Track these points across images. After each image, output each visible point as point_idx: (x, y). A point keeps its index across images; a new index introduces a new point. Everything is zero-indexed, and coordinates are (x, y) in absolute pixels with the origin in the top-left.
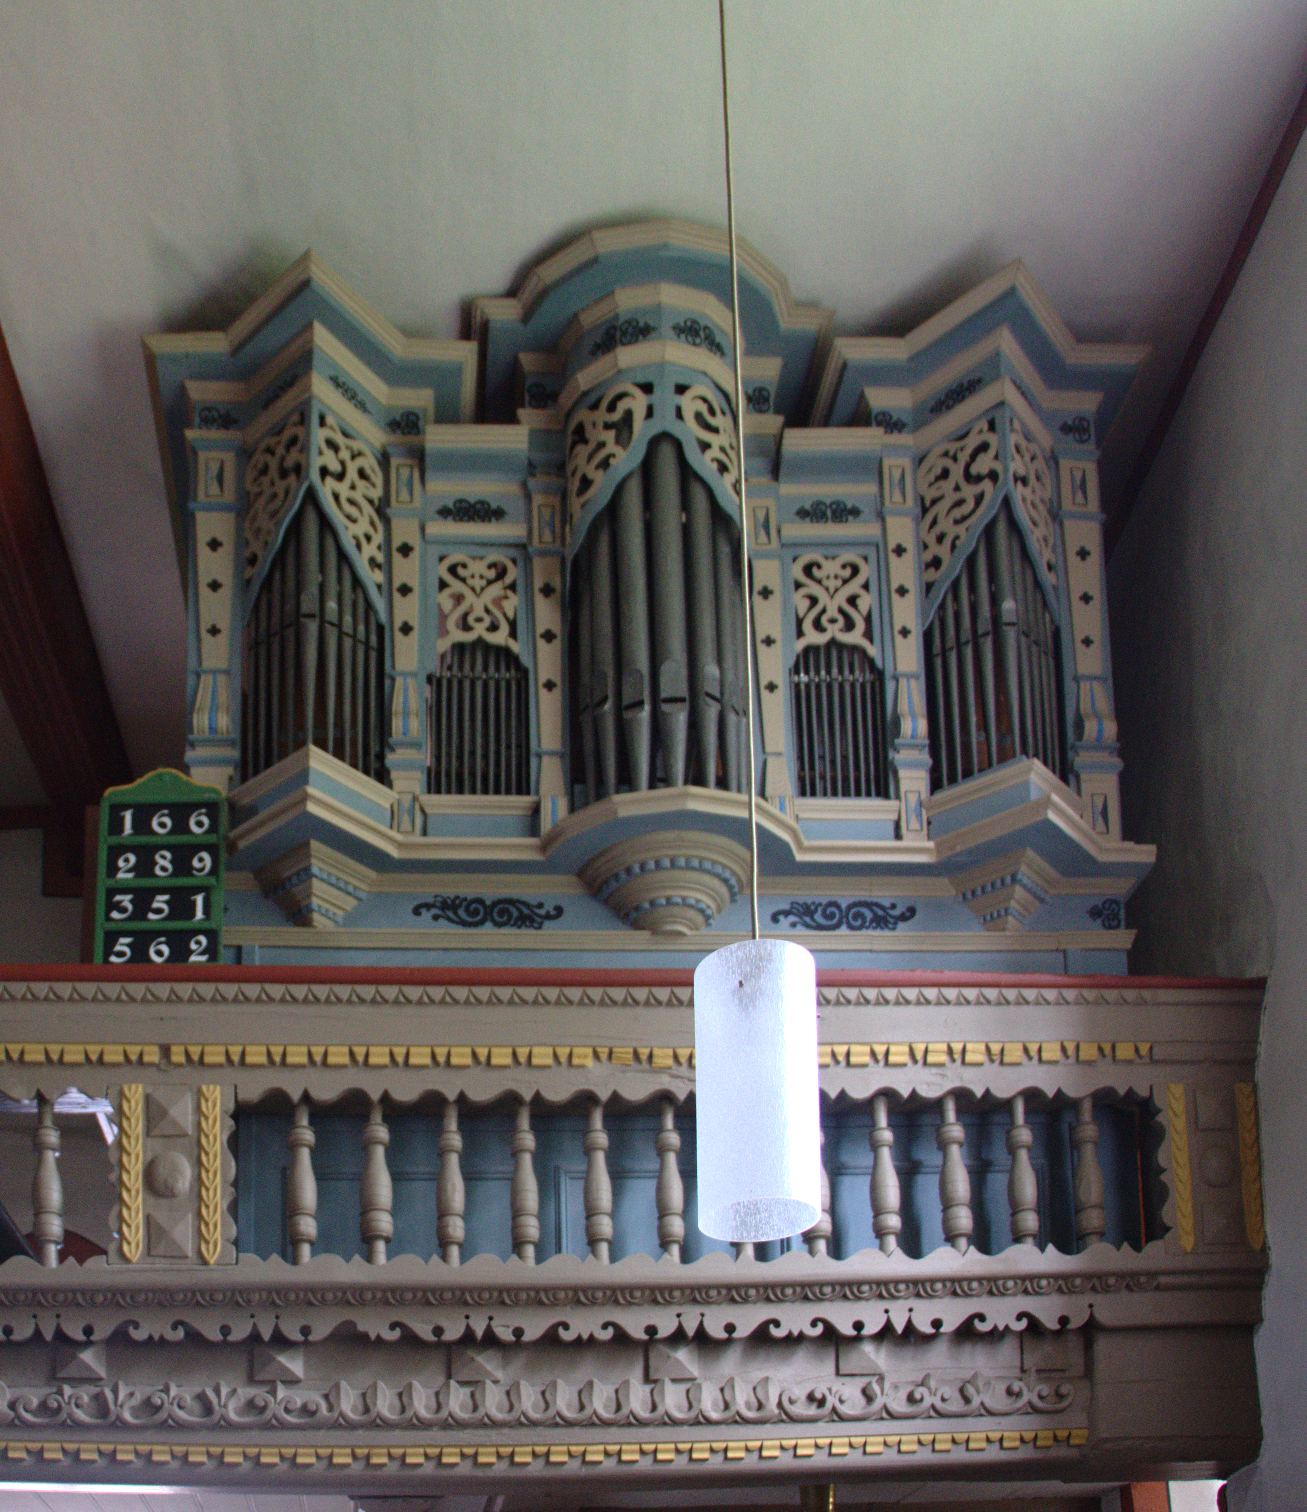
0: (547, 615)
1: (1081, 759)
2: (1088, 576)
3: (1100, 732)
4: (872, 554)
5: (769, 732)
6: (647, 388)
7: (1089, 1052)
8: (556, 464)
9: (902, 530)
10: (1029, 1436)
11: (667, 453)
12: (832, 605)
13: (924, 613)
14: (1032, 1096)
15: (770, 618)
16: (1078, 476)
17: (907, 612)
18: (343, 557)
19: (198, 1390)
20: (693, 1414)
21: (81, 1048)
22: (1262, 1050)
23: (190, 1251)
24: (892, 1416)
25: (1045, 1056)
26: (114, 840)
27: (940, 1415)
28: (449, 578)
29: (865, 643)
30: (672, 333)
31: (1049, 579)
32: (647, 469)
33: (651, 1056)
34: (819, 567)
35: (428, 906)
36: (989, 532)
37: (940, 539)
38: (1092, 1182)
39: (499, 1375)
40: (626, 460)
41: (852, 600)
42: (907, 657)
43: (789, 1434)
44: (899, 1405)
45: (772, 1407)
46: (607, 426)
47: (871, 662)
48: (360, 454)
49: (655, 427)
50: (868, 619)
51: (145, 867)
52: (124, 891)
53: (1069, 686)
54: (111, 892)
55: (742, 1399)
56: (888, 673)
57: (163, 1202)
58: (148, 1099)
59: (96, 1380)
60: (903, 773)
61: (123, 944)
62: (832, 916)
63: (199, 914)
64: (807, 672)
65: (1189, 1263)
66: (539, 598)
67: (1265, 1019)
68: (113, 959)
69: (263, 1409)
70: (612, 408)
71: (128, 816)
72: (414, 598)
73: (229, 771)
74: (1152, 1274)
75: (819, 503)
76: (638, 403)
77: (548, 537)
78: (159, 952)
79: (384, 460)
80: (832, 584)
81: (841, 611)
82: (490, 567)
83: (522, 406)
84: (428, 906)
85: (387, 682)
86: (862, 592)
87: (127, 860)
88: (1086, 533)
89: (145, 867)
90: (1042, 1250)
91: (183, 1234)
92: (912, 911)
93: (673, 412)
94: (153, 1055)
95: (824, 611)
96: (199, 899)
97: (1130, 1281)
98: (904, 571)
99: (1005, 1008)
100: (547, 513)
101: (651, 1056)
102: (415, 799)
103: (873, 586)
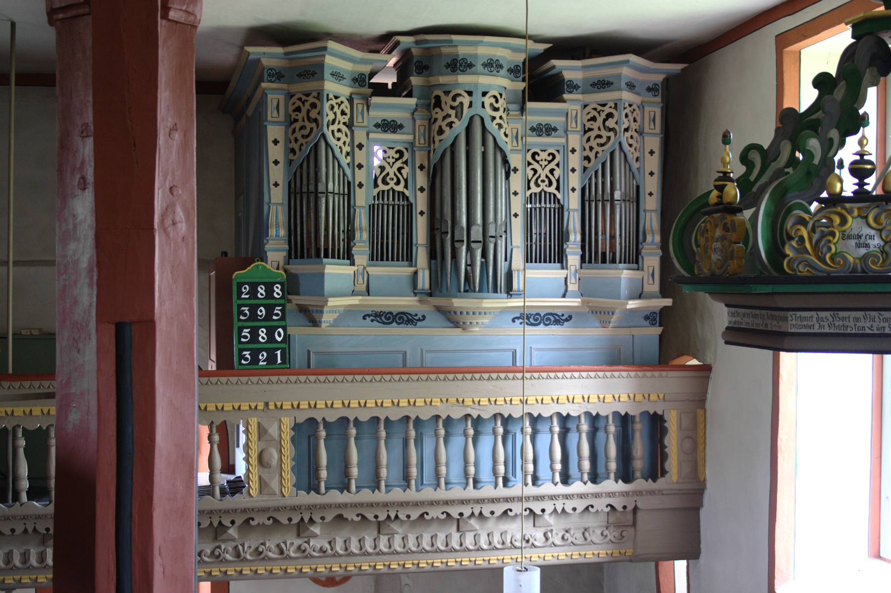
0: (421, 179)
2: (653, 163)
3: (653, 240)
6: (470, 93)
7: (639, 397)
8: (433, 129)
9: (575, 140)
11: (477, 122)
12: (543, 173)
13: (582, 181)
14: (616, 414)
17: (575, 181)
19: (277, 542)
20: (476, 547)
21: (231, 404)
22: (709, 396)
23: (277, 492)
31: (635, 166)
33: (463, 401)
35: (369, 315)
38: (639, 448)
39: (399, 531)
40: (460, 127)
41: (552, 171)
42: (574, 202)
44: (558, 541)
45: (508, 544)
46: (452, 108)
49: (473, 112)
50: (558, 181)
53: (642, 213)
56: (565, 209)
57: (266, 470)
58: (259, 424)
59: (233, 540)
60: (569, 257)
62: (537, 319)
64: (531, 203)
65: (675, 487)
66: (418, 170)
67: (711, 383)
69: (304, 551)
70: (454, 99)
73: (285, 254)
74: (660, 491)
76: (466, 100)
77: (422, 141)
79: (350, 100)
80: (544, 163)
82: (396, 152)
83: (413, 75)
84: (369, 315)
85: (352, 210)
86: (556, 168)
87: (263, 355)
88: (654, 143)
90: (617, 482)
91: (274, 484)
94: (261, 406)
95: (539, 177)
97: (652, 493)
98: (575, 161)
99: (606, 380)
100: (422, 129)
101: (463, 401)
102: (364, 268)
103: (561, 165)
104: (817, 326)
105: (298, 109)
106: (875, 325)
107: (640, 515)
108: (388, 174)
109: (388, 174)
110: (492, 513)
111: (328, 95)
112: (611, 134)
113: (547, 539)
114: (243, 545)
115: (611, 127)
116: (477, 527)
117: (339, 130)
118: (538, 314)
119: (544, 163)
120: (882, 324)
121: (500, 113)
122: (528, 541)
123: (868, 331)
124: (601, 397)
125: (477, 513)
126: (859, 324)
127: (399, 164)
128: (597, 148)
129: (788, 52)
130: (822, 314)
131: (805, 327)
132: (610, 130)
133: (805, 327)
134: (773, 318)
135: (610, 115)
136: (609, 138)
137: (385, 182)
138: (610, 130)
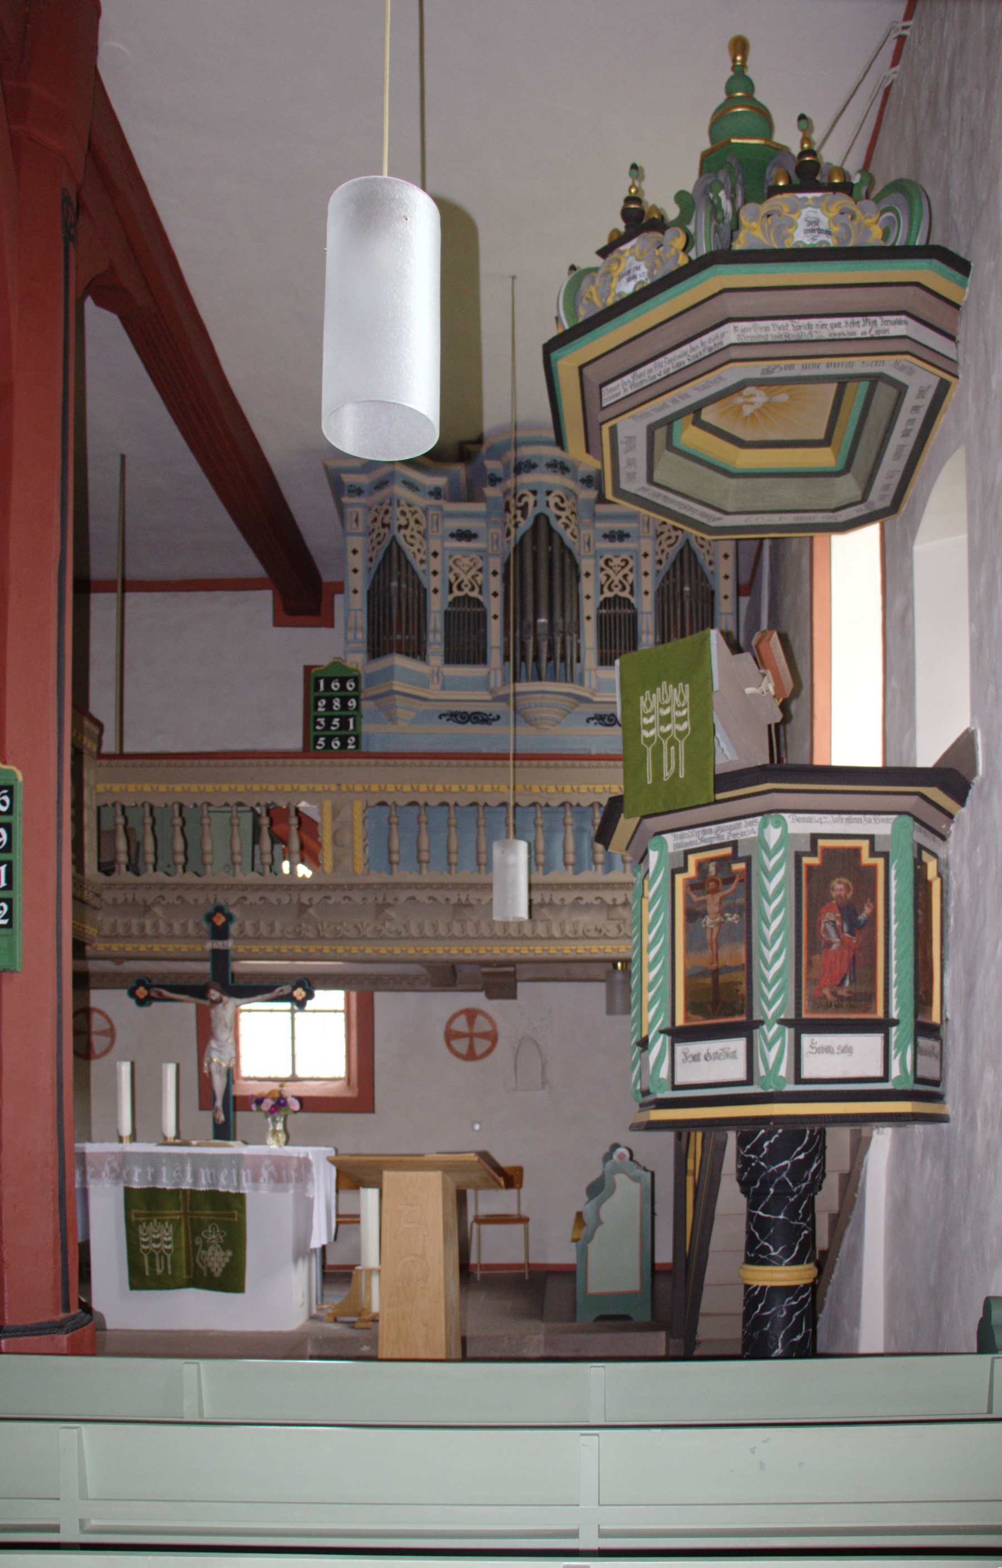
6: (534, 493)
12: (616, 578)
15: (587, 586)
17: (649, 584)
18: (407, 562)
26: (317, 694)
28: (453, 566)
30: (545, 468)
34: (611, 561)
36: (681, 552)
37: (663, 551)
41: (625, 576)
45: (580, 933)
46: (517, 508)
48: (416, 512)
49: (538, 510)
50: (632, 586)
51: (329, 706)
52: (321, 717)
54: (316, 718)
61: (321, 741)
63: (351, 727)
68: (318, 747)
69: (380, 931)
70: (520, 500)
71: (322, 682)
72: (438, 577)
75: (612, 532)
76: (530, 499)
78: (336, 744)
80: (617, 569)
81: (620, 582)
83: (485, 486)
89: (329, 706)
93: (545, 504)
94: (334, 788)
96: (351, 720)
98: (647, 565)
101: (530, 788)
102: (439, 668)
103: (635, 570)
105: (375, 520)
106: (662, 369)
108: (462, 581)
109: (462, 581)
111: (398, 502)
112: (679, 533)
113: (620, 930)
114: (322, 924)
117: (412, 537)
119: (617, 569)
121: (567, 513)
123: (658, 378)
127: (473, 572)
131: (614, 396)
133: (614, 396)
136: (677, 537)
137: (459, 588)
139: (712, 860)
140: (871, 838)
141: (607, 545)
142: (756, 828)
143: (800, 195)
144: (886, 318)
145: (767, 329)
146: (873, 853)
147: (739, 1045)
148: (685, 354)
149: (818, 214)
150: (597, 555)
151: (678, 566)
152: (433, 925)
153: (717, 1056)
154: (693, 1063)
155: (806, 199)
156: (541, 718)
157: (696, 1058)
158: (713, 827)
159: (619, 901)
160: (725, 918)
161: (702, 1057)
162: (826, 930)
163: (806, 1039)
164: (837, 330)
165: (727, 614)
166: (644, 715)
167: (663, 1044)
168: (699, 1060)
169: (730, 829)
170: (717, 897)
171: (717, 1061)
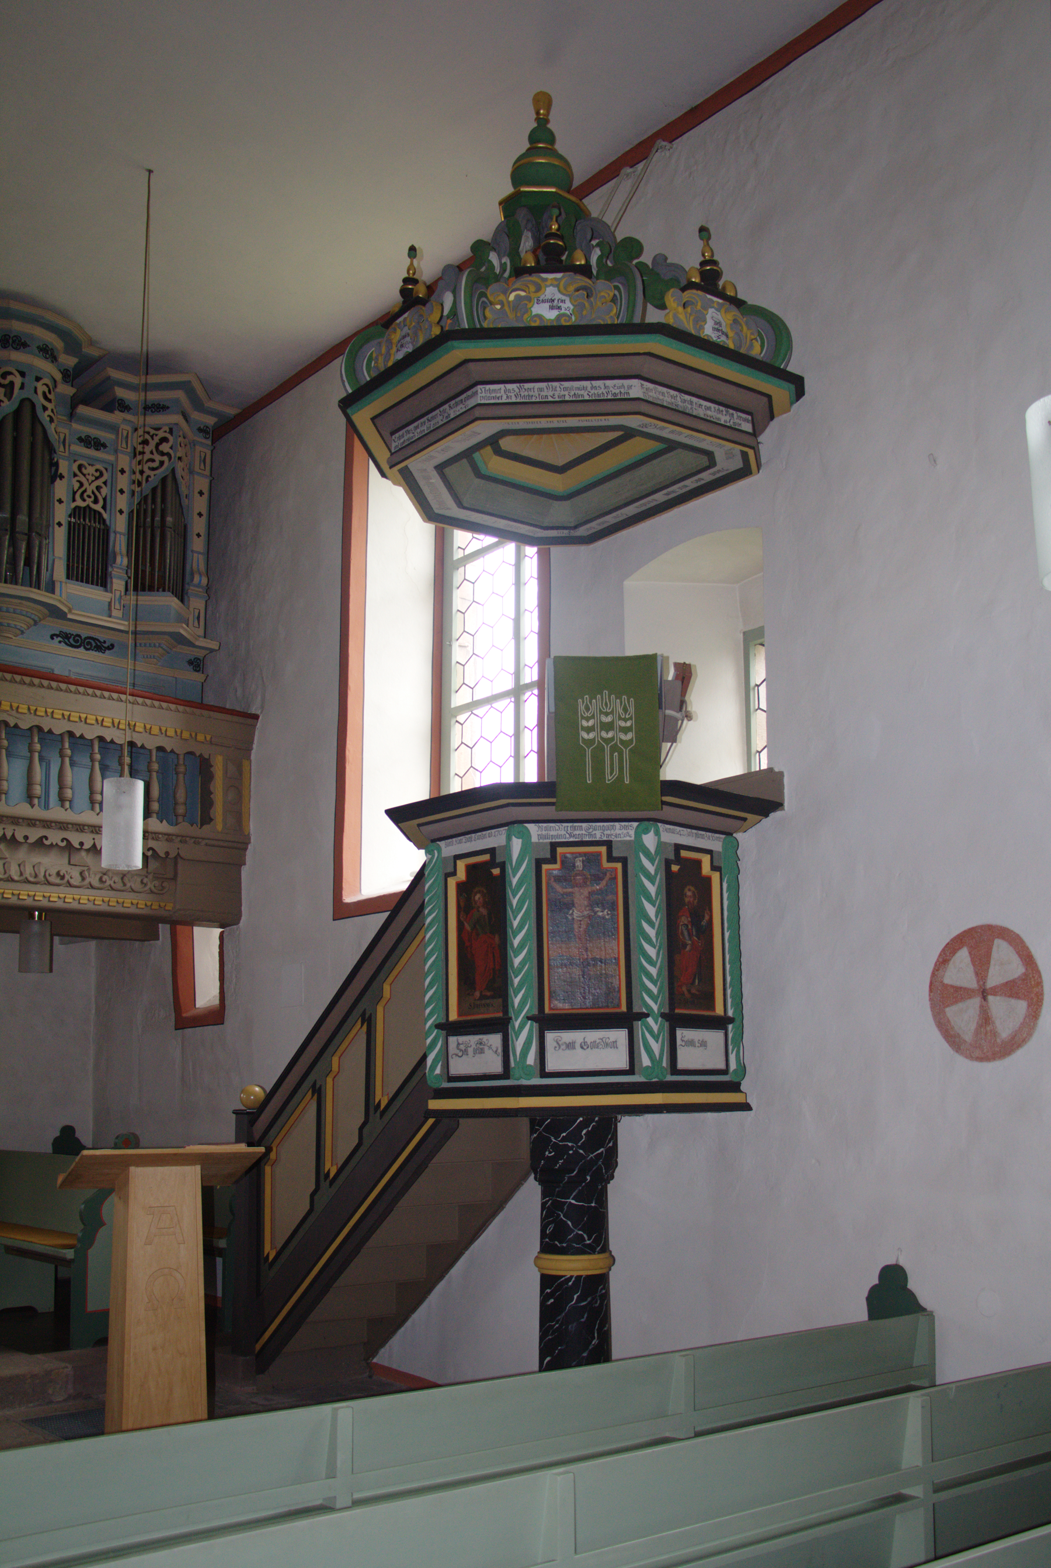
1: (191, 589)
4: (110, 469)
5: (58, 546)
6: (23, 374)
7: (186, 735)
10: (149, 903)
11: (27, 404)
12: (90, 489)
14: (160, 749)
16: (203, 456)
17: (122, 502)
24: (92, 887)
25: (168, 734)
27: (113, 889)
29: (102, 511)
32: (17, 413)
36: (164, 480)
41: (98, 488)
42: (120, 524)
43: (48, 891)
44: (96, 883)
47: (104, 521)
49: (25, 395)
50: (105, 499)
53: (189, 553)
55: (28, 871)
56: (112, 530)
60: (114, 580)
62: (77, 641)
76: (18, 380)
80: (91, 478)
81: (93, 492)
92: (112, 646)
95: (85, 491)
97: (197, 841)
98: (123, 482)
103: (109, 484)
104: (505, 397)
106: (557, 394)
107: (180, 862)
110: (26, 838)
112: (165, 458)
113: (83, 879)
115: (165, 451)
116: (7, 854)
118: (79, 636)
120: (563, 393)
122: (63, 878)
123: (550, 399)
124: (148, 727)
125: (9, 835)
126: (542, 394)
128: (147, 472)
129: (130, 791)
130: (509, 386)
131: (494, 398)
132: (162, 454)
133: (494, 398)
134: (457, 404)
135: (164, 440)
136: (162, 463)
138: (162, 454)
139: (580, 854)
140: (608, 844)
141: (79, 449)
142: (632, 833)
143: (709, 296)
144: (740, 414)
145: (663, 394)
146: (611, 858)
147: (620, 1036)
148: (584, 388)
149: (719, 317)
150: (74, 457)
151: (159, 491)
152: (19, 865)
153: (594, 1045)
154: (568, 1051)
155: (713, 302)
156: (9, 625)
157: (570, 1046)
158: (584, 825)
159: (87, 846)
160: (595, 913)
161: (577, 1045)
162: (682, 933)
163: (680, 1033)
164: (709, 413)
165: (199, 553)
166: (583, 718)
167: (531, 1030)
168: (574, 1048)
169: (603, 829)
170: (585, 892)
171: (595, 1050)
